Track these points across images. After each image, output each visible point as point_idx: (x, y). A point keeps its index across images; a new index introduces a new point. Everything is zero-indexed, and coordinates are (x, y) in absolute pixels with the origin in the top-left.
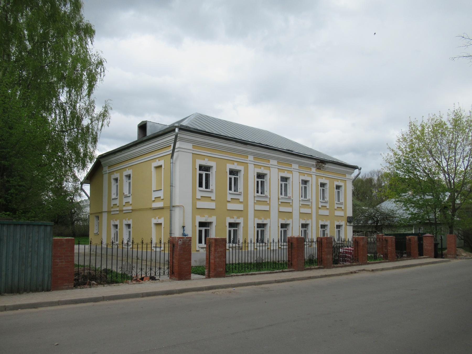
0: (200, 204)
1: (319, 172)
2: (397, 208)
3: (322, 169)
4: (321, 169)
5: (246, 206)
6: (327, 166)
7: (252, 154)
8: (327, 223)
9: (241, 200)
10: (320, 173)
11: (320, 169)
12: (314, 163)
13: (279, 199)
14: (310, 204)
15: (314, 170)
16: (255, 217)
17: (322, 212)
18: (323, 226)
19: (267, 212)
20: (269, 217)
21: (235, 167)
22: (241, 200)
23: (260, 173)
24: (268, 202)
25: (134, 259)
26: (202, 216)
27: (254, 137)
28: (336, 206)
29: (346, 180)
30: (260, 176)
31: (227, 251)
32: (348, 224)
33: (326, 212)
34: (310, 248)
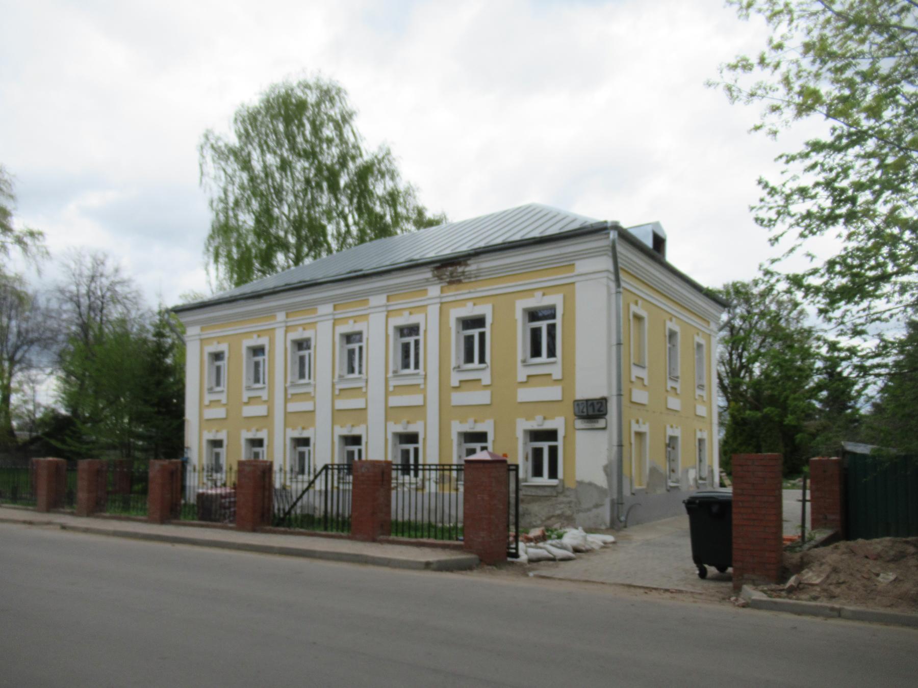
0: (458, 398)
1: (457, 290)
2: (862, 321)
3: (467, 281)
4: (464, 281)
5: (270, 410)
6: (473, 266)
7: (280, 308)
8: (222, 435)
9: (224, 401)
10: (452, 294)
11: (459, 282)
12: (427, 274)
13: (367, 381)
14: (421, 381)
15: (434, 291)
16: (286, 425)
17: (210, 414)
18: (217, 443)
19: (310, 414)
20: (364, 421)
21: (255, 342)
22: (555, 377)
23: (467, 317)
24: (312, 394)
25: (523, 501)
26: (529, 417)
27: (437, 246)
28: (245, 395)
29: (573, 283)
30: (301, 345)
31: (393, 493)
32: (579, 424)
33: (220, 412)
34: (420, 493)
